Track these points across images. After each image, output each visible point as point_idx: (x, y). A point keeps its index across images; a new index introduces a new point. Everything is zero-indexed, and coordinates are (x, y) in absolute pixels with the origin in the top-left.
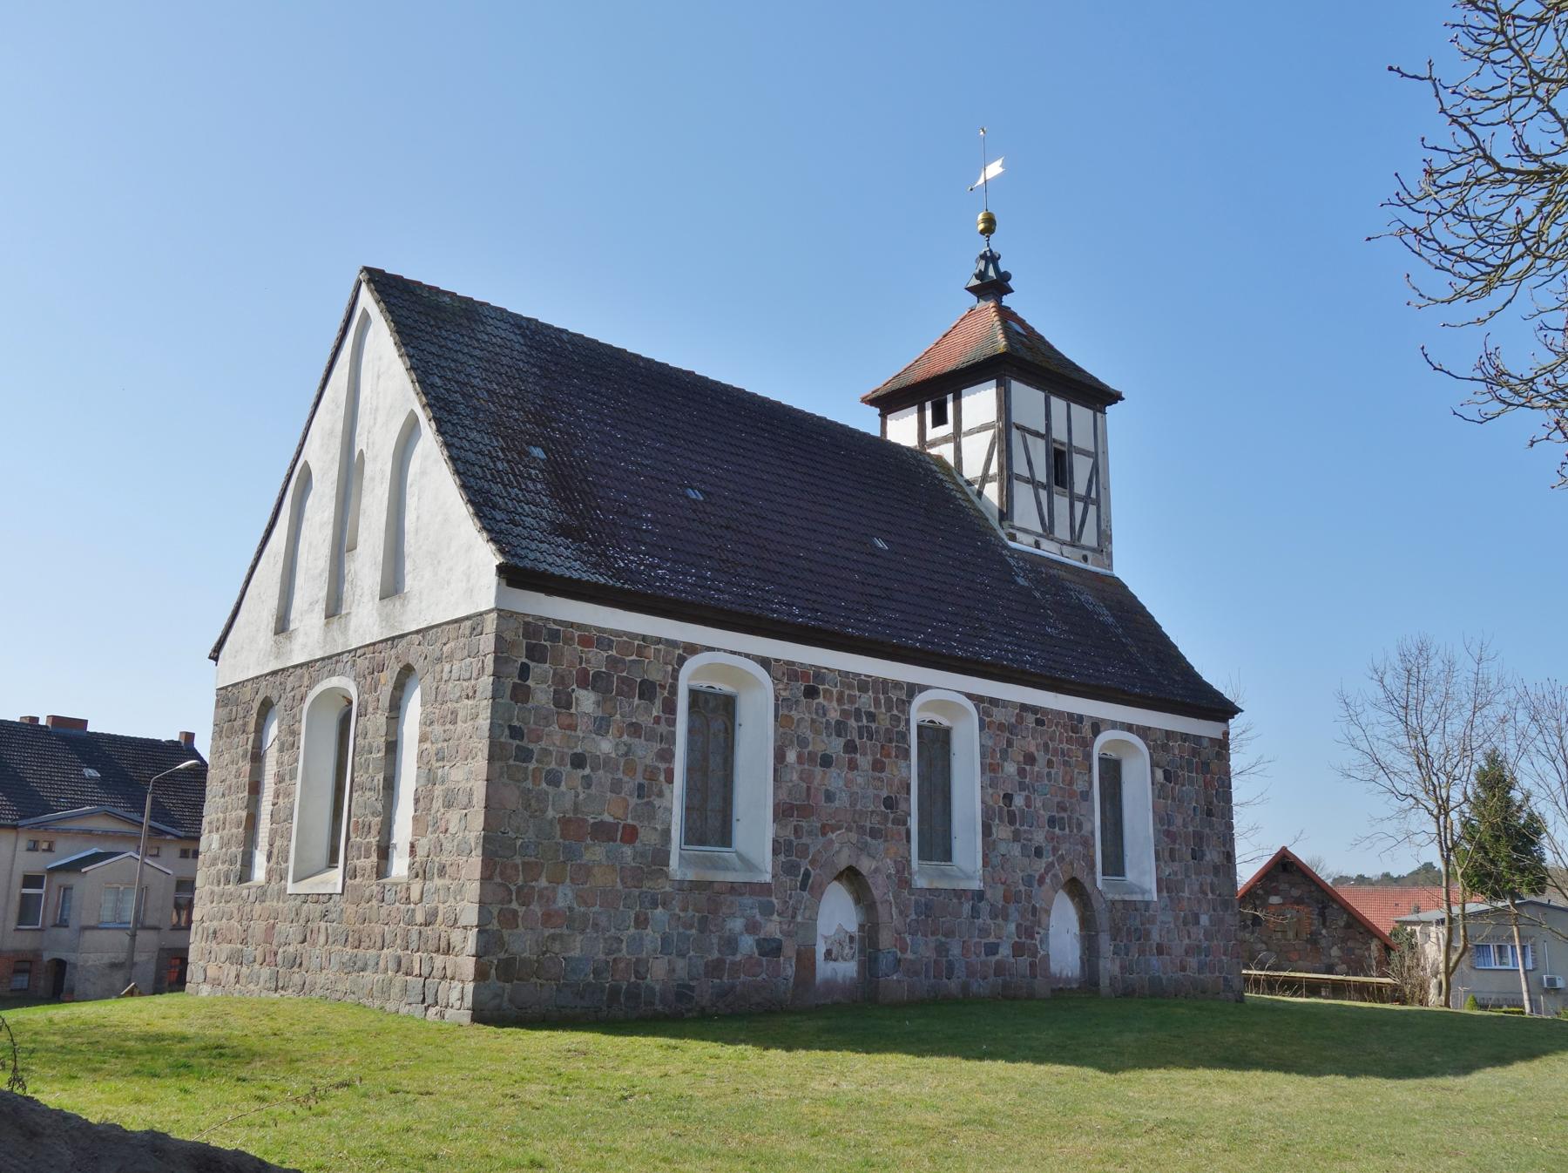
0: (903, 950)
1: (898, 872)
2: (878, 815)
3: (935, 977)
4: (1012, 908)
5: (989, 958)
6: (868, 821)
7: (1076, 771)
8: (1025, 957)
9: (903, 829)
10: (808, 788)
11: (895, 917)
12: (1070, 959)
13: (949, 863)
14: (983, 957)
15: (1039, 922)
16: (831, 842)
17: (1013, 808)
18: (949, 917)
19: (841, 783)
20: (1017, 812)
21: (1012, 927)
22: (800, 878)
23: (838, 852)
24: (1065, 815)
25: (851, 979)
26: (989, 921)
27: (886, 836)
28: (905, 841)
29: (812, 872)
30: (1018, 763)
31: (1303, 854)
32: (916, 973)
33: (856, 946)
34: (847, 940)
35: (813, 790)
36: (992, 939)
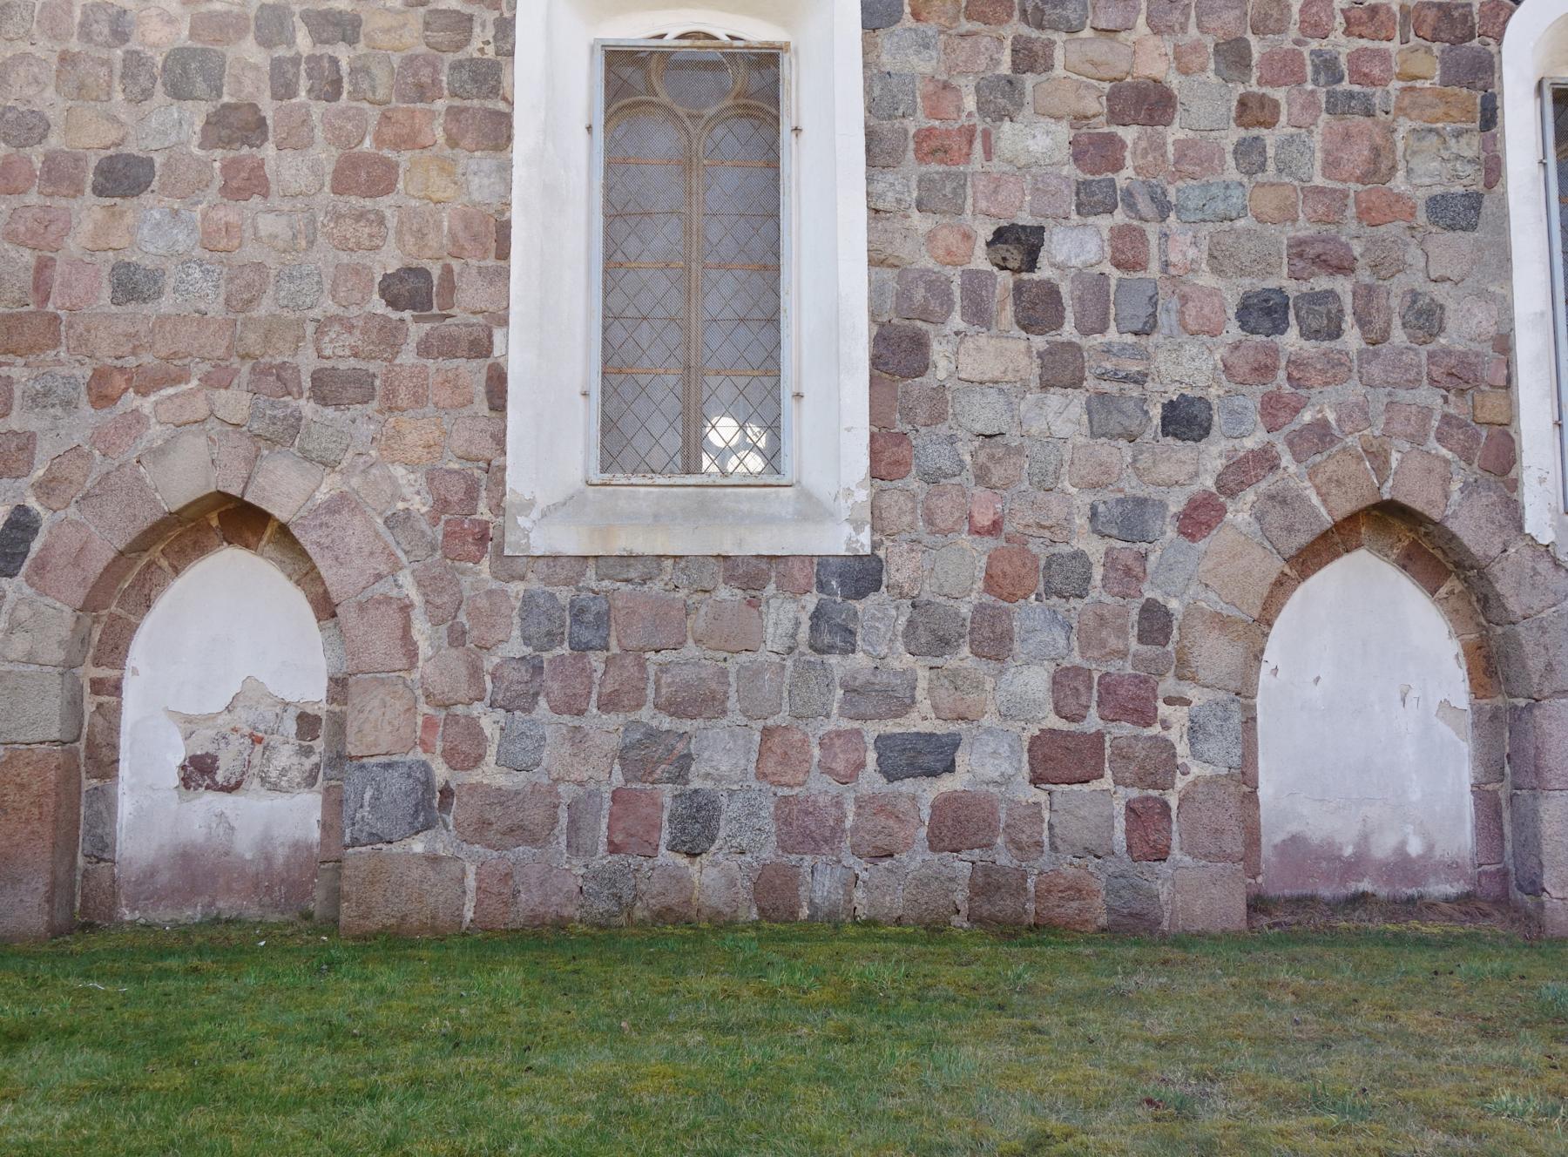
0: (465, 755)
1: (442, 505)
2: (350, 328)
3: (614, 848)
4: (1029, 615)
5: (907, 786)
6: (311, 352)
7: (1404, 126)
8: (1107, 782)
9: (473, 373)
10: (43, 266)
11: (424, 649)
12: (1415, 796)
14: (871, 780)
15: (1182, 663)
16: (137, 419)
17: (1044, 272)
19: (182, 239)
20: (1065, 289)
21: (1034, 681)
23: (159, 453)
24: (1343, 286)
26: (903, 660)
27: (391, 394)
29: (46, 517)
30: (1080, 119)
31: (632, 30)
32: (518, 832)
35: (60, 271)
36: (921, 721)
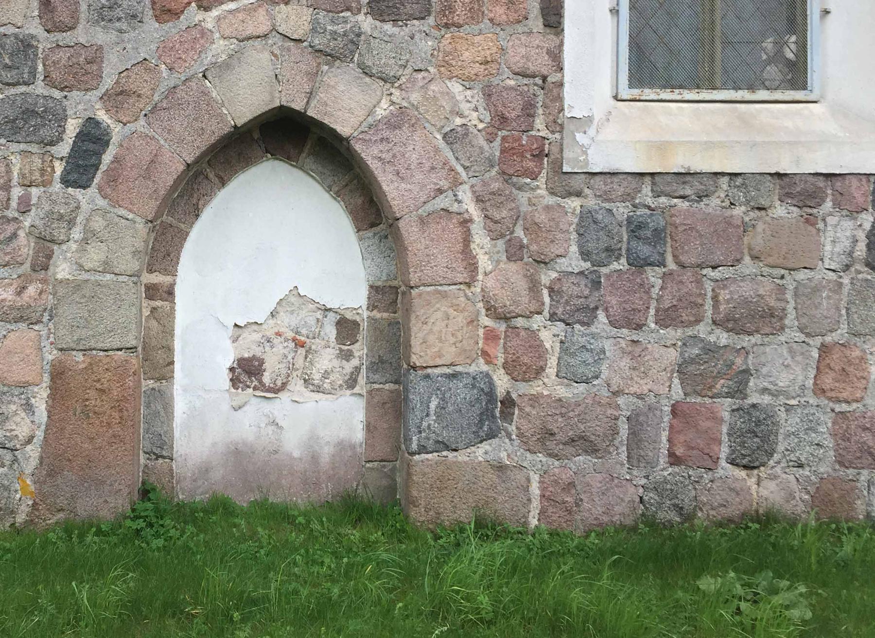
13: (799, 95)
18: (748, 266)
22: (64, 149)
23: (226, 66)
25: (342, 446)
28: (536, 23)
29: (117, 132)
33: (360, 350)
34: (331, 331)
